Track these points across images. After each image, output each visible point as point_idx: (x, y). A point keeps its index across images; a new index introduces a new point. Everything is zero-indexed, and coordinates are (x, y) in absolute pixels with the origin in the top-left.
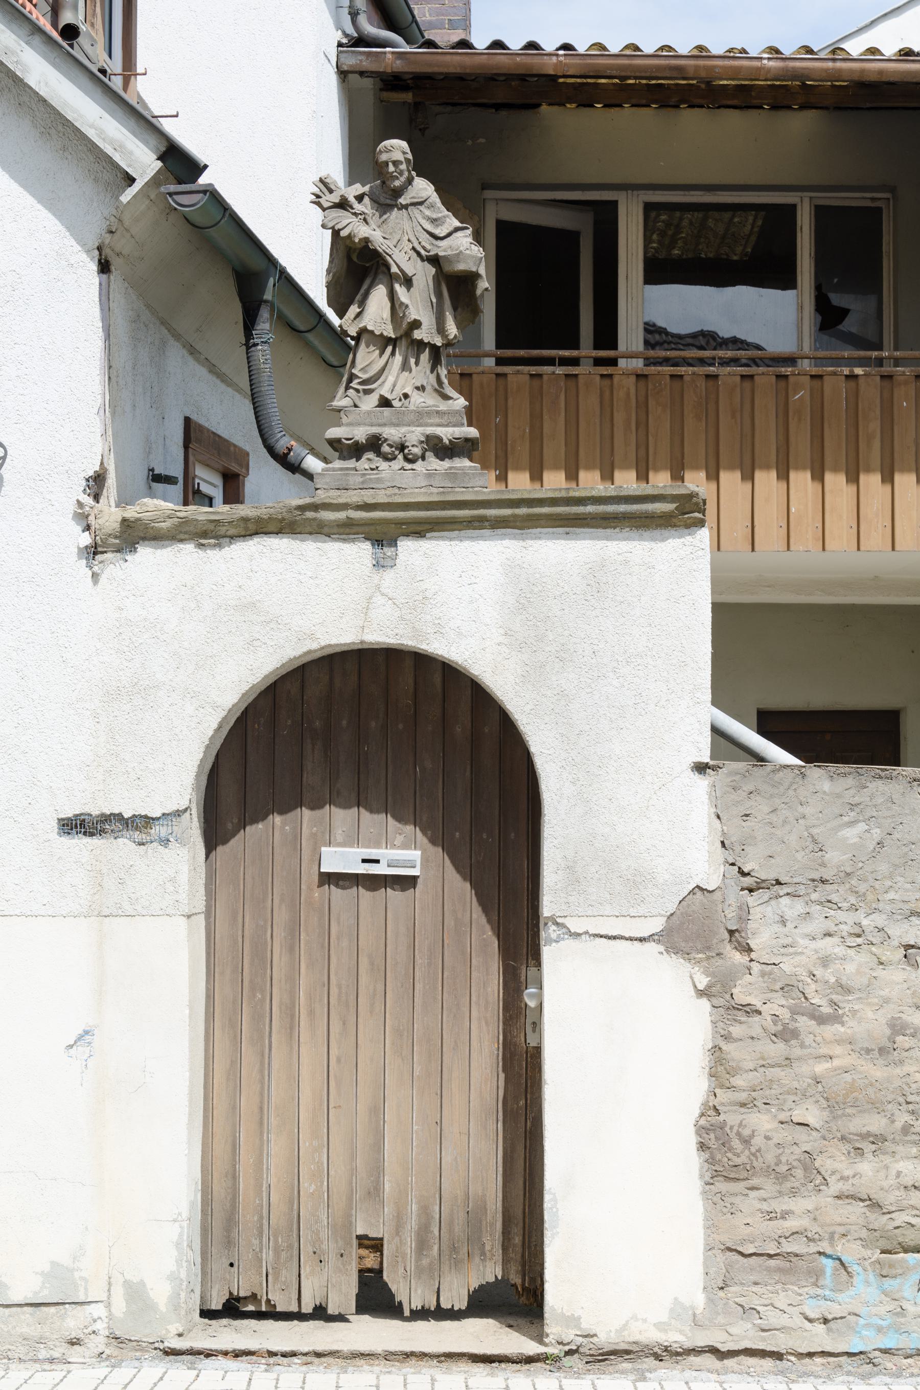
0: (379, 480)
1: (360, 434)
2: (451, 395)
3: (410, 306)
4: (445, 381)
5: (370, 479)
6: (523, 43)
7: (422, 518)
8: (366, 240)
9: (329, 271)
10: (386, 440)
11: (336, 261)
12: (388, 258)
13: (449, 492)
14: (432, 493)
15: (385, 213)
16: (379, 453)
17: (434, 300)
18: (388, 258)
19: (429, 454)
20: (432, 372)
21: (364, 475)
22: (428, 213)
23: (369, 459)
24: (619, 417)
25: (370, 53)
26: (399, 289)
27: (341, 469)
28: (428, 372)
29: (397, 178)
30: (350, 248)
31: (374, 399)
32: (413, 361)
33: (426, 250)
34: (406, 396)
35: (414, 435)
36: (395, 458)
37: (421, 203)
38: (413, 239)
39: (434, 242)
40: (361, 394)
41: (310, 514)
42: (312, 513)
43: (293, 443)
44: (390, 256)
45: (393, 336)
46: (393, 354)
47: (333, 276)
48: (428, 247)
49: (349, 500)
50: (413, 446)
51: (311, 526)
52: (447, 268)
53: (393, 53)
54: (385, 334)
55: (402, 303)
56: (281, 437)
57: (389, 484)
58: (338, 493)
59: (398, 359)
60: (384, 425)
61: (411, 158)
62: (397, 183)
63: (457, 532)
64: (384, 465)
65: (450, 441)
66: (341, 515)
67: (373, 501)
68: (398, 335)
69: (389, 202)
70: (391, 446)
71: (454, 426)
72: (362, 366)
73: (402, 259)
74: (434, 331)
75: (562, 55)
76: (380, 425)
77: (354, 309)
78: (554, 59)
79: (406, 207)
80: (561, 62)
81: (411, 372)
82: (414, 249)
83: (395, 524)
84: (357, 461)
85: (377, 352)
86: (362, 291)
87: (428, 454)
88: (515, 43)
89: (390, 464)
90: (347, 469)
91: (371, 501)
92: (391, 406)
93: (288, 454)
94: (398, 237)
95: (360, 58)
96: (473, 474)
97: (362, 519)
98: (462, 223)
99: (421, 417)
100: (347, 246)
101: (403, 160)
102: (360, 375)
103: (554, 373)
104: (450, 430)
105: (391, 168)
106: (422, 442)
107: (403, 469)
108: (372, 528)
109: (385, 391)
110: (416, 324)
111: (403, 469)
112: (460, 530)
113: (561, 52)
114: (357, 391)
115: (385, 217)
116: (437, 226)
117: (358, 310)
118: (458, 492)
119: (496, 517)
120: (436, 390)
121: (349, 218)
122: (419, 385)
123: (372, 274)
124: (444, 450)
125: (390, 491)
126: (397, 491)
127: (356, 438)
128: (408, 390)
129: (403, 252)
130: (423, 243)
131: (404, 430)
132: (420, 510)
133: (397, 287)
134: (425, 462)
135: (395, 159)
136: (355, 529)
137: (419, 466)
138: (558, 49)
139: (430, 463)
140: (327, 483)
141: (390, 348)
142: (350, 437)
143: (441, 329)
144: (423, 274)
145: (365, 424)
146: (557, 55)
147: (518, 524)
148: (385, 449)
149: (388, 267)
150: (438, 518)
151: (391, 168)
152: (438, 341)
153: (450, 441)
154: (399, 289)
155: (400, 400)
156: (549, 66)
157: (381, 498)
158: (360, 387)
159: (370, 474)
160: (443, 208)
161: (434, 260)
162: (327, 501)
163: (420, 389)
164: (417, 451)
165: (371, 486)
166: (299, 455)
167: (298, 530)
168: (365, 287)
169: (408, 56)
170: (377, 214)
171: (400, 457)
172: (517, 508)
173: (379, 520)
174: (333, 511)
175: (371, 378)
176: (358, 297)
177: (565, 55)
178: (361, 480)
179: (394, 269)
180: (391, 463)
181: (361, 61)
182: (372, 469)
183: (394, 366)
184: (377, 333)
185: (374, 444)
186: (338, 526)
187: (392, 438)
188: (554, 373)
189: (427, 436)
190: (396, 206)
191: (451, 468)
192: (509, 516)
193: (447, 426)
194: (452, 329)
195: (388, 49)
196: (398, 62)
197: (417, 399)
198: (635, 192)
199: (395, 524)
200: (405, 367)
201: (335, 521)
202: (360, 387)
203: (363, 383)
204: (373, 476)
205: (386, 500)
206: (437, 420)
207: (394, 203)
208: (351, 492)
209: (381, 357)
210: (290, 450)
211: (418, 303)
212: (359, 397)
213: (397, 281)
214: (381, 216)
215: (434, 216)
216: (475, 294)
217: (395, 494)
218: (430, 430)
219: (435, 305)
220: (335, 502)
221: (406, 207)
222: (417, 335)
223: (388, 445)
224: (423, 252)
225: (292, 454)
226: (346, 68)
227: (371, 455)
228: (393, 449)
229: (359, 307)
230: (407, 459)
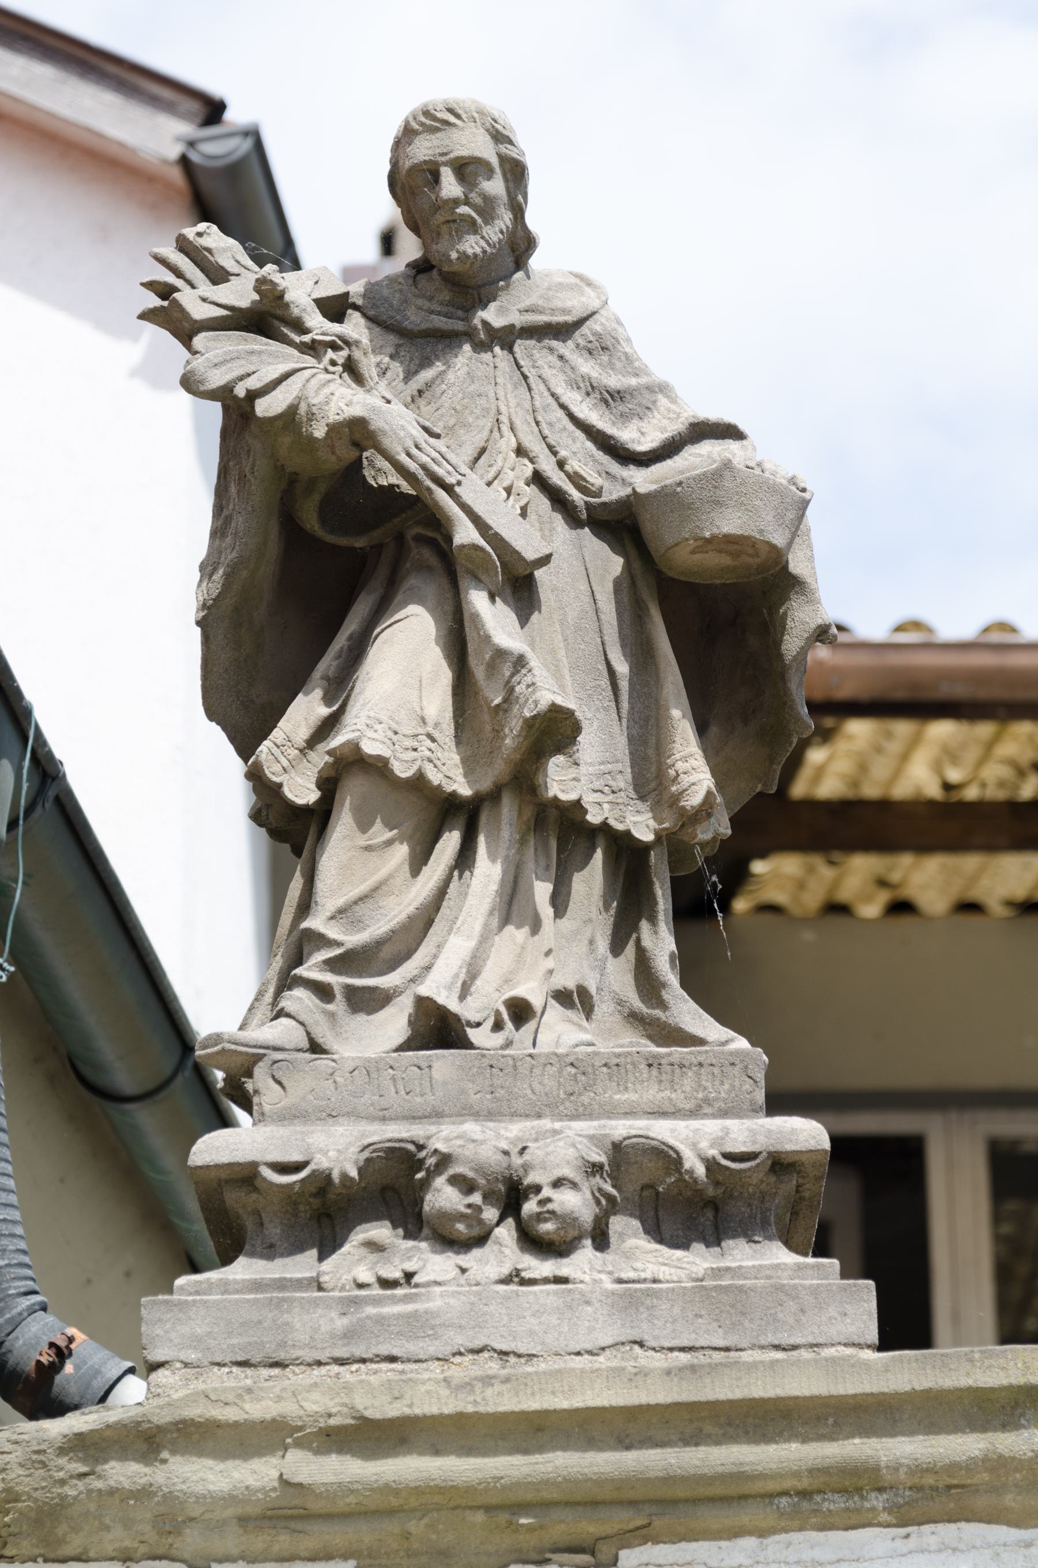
0: (417, 1324)
1: (337, 1149)
2: (698, 1031)
3: (534, 662)
4: (672, 978)
5: (381, 1320)
7: (601, 1482)
8: (358, 434)
9: (207, 569)
10: (445, 1160)
11: (239, 522)
12: (441, 495)
13: (713, 1368)
14: (642, 1373)
15: (426, 363)
16: (413, 1221)
17: (622, 668)
18: (441, 495)
19: (625, 1228)
20: (617, 948)
21: (355, 1301)
22: (587, 367)
23: (374, 1247)
26: (493, 617)
27: (257, 1286)
28: (603, 945)
29: (473, 228)
30: (293, 480)
31: (394, 1024)
32: (542, 891)
33: (583, 490)
34: (520, 1012)
35: (559, 1151)
36: (481, 1240)
37: (562, 331)
38: (537, 448)
39: (614, 467)
40: (338, 1005)
41: (123, 1473)
42: (134, 1468)
43: (72, 1331)
44: (449, 489)
45: (465, 790)
46: (465, 859)
47: (228, 576)
48: (595, 480)
49: (288, 1409)
50: (557, 1184)
51: (127, 1524)
52: (678, 545)
54: (434, 777)
55: (501, 654)
56: (32, 1311)
57: (461, 1341)
58: (245, 1377)
59: (488, 872)
60: (436, 1115)
62: (472, 245)
63: (749, 1542)
64: (434, 1264)
65: (711, 1165)
66: (257, 1474)
67: (394, 1411)
68: (486, 784)
69: (439, 322)
70: (465, 1185)
71: (724, 1114)
72: (340, 901)
73: (493, 506)
74: (624, 781)
76: (414, 1118)
77: (306, 710)
79: (505, 338)
81: (536, 926)
82: (538, 479)
83: (489, 1509)
84: (321, 1258)
85: (402, 851)
86: (340, 642)
87: (617, 1224)
89: (463, 1260)
90: (282, 1284)
91: (382, 1408)
92: (468, 1045)
93: (55, 1368)
94: (478, 440)
96: (815, 1291)
97: (346, 1489)
99: (580, 1082)
100: (279, 469)
101: (494, 161)
102: (332, 932)
104: (711, 1127)
105: (450, 186)
106: (595, 1169)
107: (515, 1277)
108: (393, 1526)
109: (440, 988)
110: (555, 731)
111: (515, 1277)
112: (762, 1533)
114: (323, 992)
115: (427, 374)
116: (625, 418)
117: (324, 711)
118: (753, 1366)
119: (919, 1469)
120: (634, 1018)
121: (286, 358)
122: (571, 985)
123: (382, 572)
124: (689, 1206)
125: (464, 1369)
126: (493, 1366)
127: (321, 1162)
128: (533, 992)
129: (498, 486)
130: (574, 465)
131: (514, 1130)
132: (591, 1444)
133: (478, 600)
134: (608, 1257)
135: (464, 152)
136: (318, 1536)
137: (583, 1263)
139: (628, 1256)
140: (196, 1342)
141: (450, 842)
142: (296, 1157)
143: (650, 779)
144: (581, 573)
145: (354, 1115)
147: (1010, 1500)
148: (443, 1197)
149: (438, 526)
150: (669, 1480)
151: (450, 186)
152: (642, 826)
153: (711, 1165)
154: (493, 617)
155: (498, 1026)
157: (429, 1395)
158: (335, 980)
159: (377, 1301)
161: (619, 525)
162: (195, 1412)
163: (575, 999)
164: (576, 1203)
165: (385, 1350)
166: (97, 1372)
167: (75, 1544)
168: (351, 626)
170: (397, 369)
171: (506, 1233)
172: (1004, 1427)
173: (418, 1491)
174: (223, 1454)
175: (379, 944)
176: (327, 664)
178: (341, 1323)
179: (465, 534)
180: (467, 1260)
182: (386, 1283)
183: (471, 901)
184: (402, 770)
185: (393, 1189)
186: (243, 1520)
187: (469, 1151)
189: (617, 1147)
190: (469, 335)
191: (717, 1273)
192: (970, 1466)
193: (694, 1113)
194: (694, 774)
197: (559, 1031)
199: (489, 1509)
200: (512, 906)
201: (230, 1499)
202: (335, 980)
203: (342, 963)
204: (394, 1307)
205: (448, 1404)
206: (652, 1093)
207: (459, 326)
208: (297, 1377)
209: (415, 872)
210: (62, 1354)
211: (564, 646)
212: (332, 1016)
214: (408, 377)
215: (613, 381)
216: (780, 656)
217: (487, 1380)
218: (621, 1128)
219: (624, 685)
220: (230, 1414)
221: (505, 338)
222: (561, 780)
223: (455, 1180)
224: (575, 495)
225: (69, 1368)
227: (381, 1231)
228: (476, 1198)
229: (328, 700)
230: (532, 1241)
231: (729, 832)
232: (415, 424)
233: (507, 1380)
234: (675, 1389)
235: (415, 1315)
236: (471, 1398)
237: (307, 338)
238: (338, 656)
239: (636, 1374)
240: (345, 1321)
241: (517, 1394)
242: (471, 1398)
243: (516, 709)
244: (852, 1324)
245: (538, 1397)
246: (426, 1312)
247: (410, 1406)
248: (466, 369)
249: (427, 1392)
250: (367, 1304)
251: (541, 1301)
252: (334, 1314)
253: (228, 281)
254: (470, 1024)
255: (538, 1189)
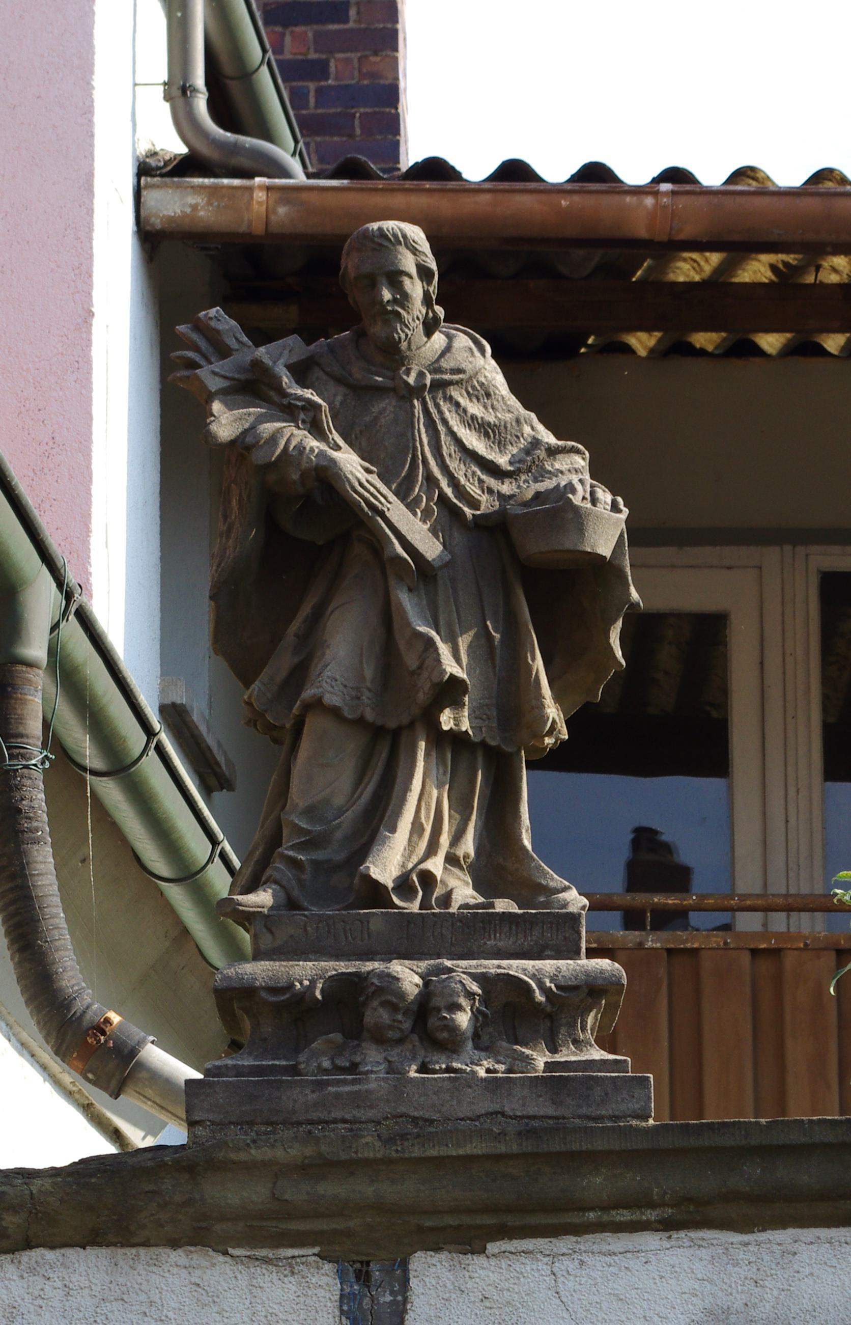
0: (358, 1099)
5: (337, 1096)
6: (574, 168)
24: (797, 1052)
25: (215, 189)
26: (407, 602)
53: (269, 189)
61: (434, 266)
75: (666, 194)
78: (649, 201)
80: (665, 207)
88: (555, 169)
90: (272, 1070)
95: (192, 200)
98: (559, 439)
103: (640, 946)
104: (548, 965)
113: (665, 187)
138: (657, 180)
146: (656, 194)
156: (640, 220)
159: (338, 1083)
160: (513, 401)
169: (305, 196)
177: (673, 193)
178: (313, 1097)
181: (194, 207)
188: (640, 946)
195: (258, 180)
196: (282, 210)
198: (801, 550)
213: (400, 578)
226: (158, 224)
231: (567, 737)
232: (360, 468)
233: (418, 1136)
234: (524, 1144)
235: (357, 1093)
236: (394, 1148)
237: (285, 401)
238: (305, 621)
239: (499, 1134)
240: (315, 1096)
241: (423, 1146)
242: (394, 1148)
243: (425, 674)
244: (637, 1103)
245: (437, 1148)
246: (367, 1091)
247: (356, 1153)
248: (392, 416)
249: (367, 1143)
250: (329, 1085)
251: (440, 1085)
252: (307, 1091)
253: (231, 355)
254: (228, 78)
255: (439, 1010)
